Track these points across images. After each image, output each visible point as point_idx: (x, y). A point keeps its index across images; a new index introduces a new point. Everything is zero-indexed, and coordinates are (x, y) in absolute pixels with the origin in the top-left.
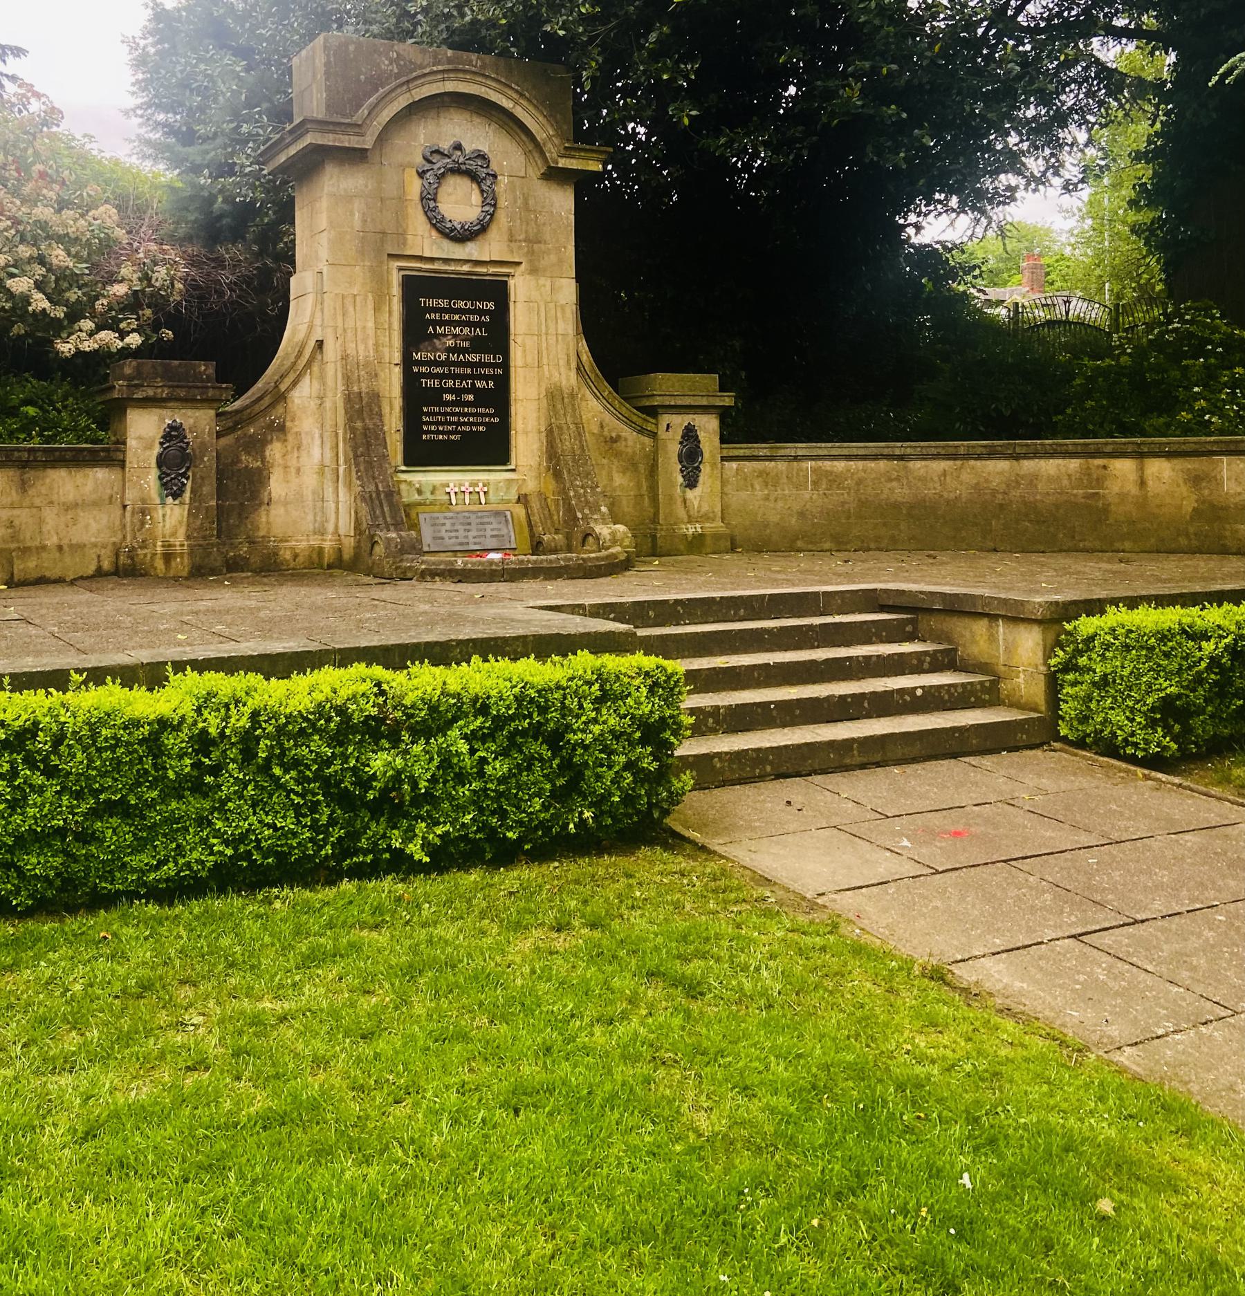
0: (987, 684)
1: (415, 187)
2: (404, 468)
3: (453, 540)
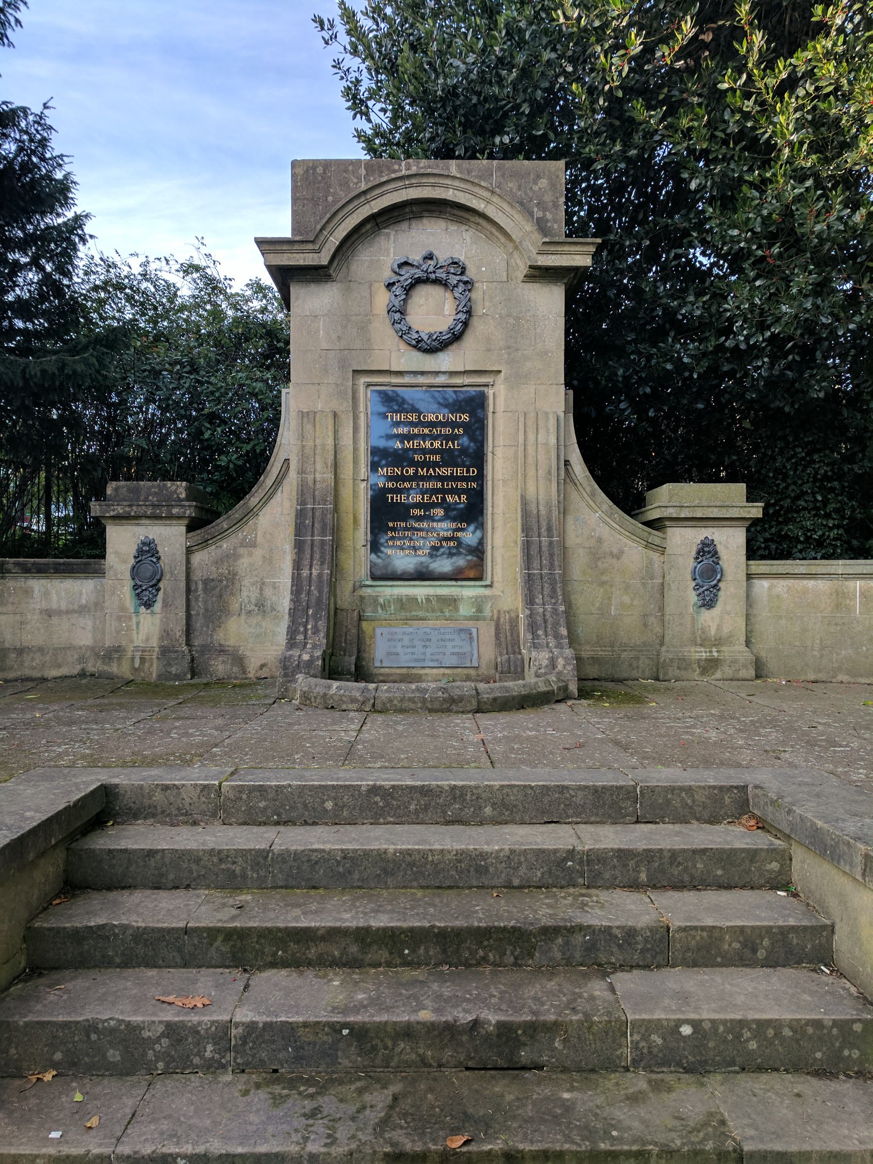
0: (858, 1027)
1: (383, 299)
2: (368, 583)
3: (409, 657)
